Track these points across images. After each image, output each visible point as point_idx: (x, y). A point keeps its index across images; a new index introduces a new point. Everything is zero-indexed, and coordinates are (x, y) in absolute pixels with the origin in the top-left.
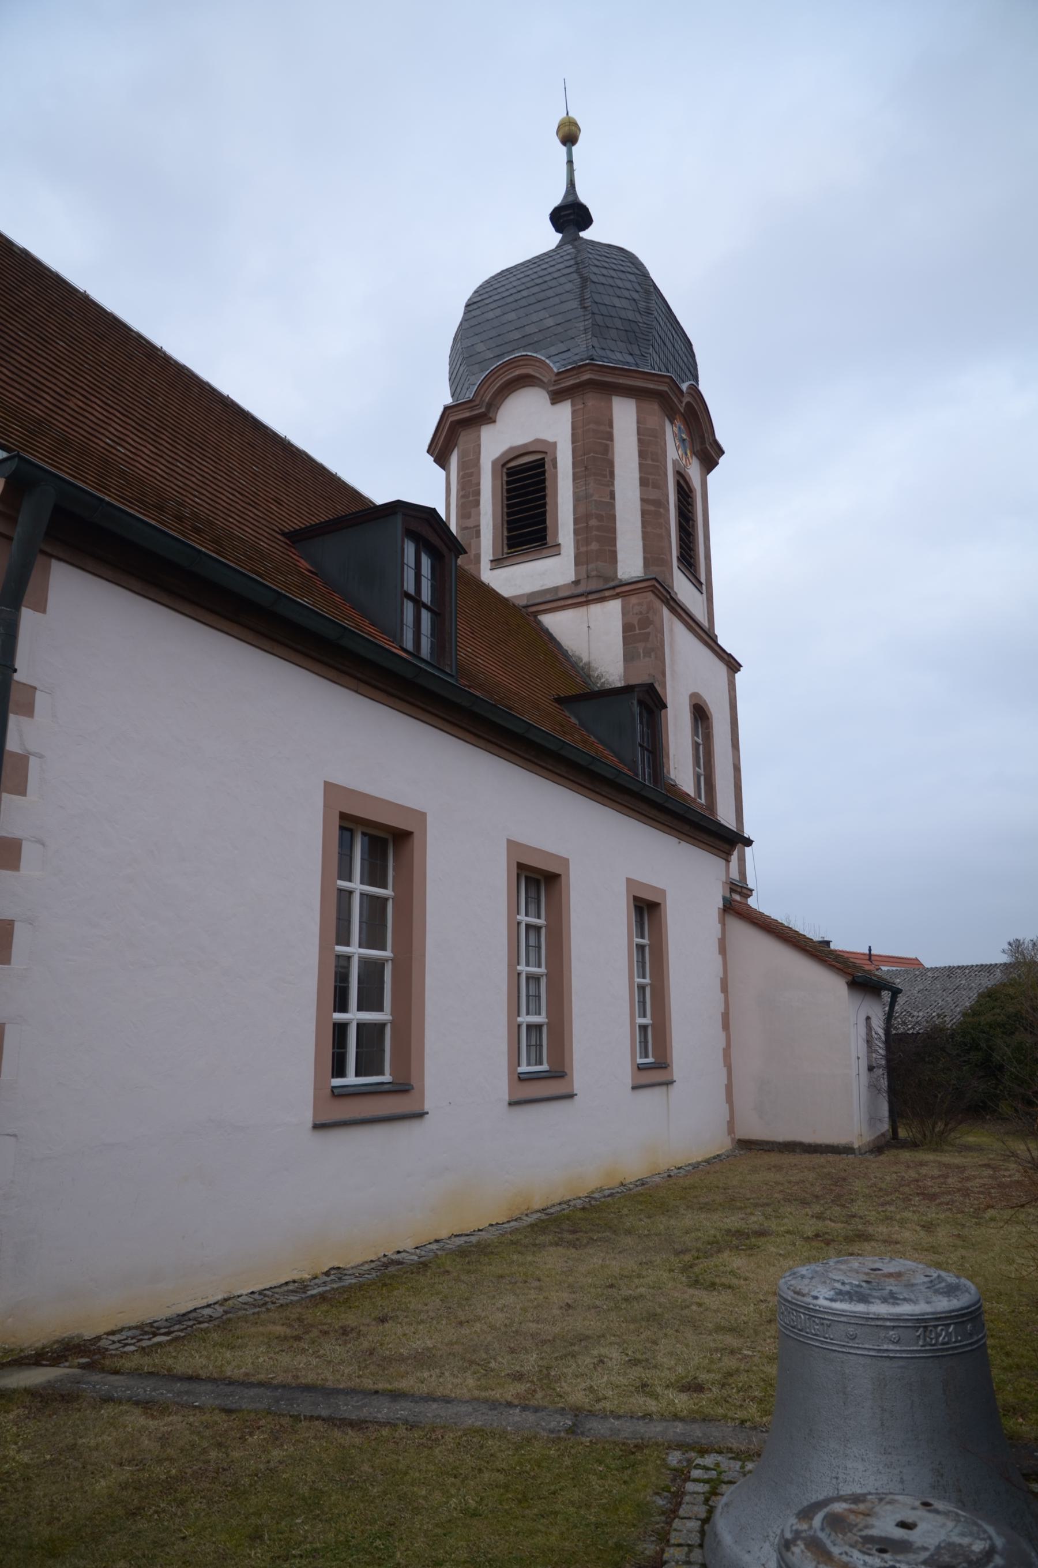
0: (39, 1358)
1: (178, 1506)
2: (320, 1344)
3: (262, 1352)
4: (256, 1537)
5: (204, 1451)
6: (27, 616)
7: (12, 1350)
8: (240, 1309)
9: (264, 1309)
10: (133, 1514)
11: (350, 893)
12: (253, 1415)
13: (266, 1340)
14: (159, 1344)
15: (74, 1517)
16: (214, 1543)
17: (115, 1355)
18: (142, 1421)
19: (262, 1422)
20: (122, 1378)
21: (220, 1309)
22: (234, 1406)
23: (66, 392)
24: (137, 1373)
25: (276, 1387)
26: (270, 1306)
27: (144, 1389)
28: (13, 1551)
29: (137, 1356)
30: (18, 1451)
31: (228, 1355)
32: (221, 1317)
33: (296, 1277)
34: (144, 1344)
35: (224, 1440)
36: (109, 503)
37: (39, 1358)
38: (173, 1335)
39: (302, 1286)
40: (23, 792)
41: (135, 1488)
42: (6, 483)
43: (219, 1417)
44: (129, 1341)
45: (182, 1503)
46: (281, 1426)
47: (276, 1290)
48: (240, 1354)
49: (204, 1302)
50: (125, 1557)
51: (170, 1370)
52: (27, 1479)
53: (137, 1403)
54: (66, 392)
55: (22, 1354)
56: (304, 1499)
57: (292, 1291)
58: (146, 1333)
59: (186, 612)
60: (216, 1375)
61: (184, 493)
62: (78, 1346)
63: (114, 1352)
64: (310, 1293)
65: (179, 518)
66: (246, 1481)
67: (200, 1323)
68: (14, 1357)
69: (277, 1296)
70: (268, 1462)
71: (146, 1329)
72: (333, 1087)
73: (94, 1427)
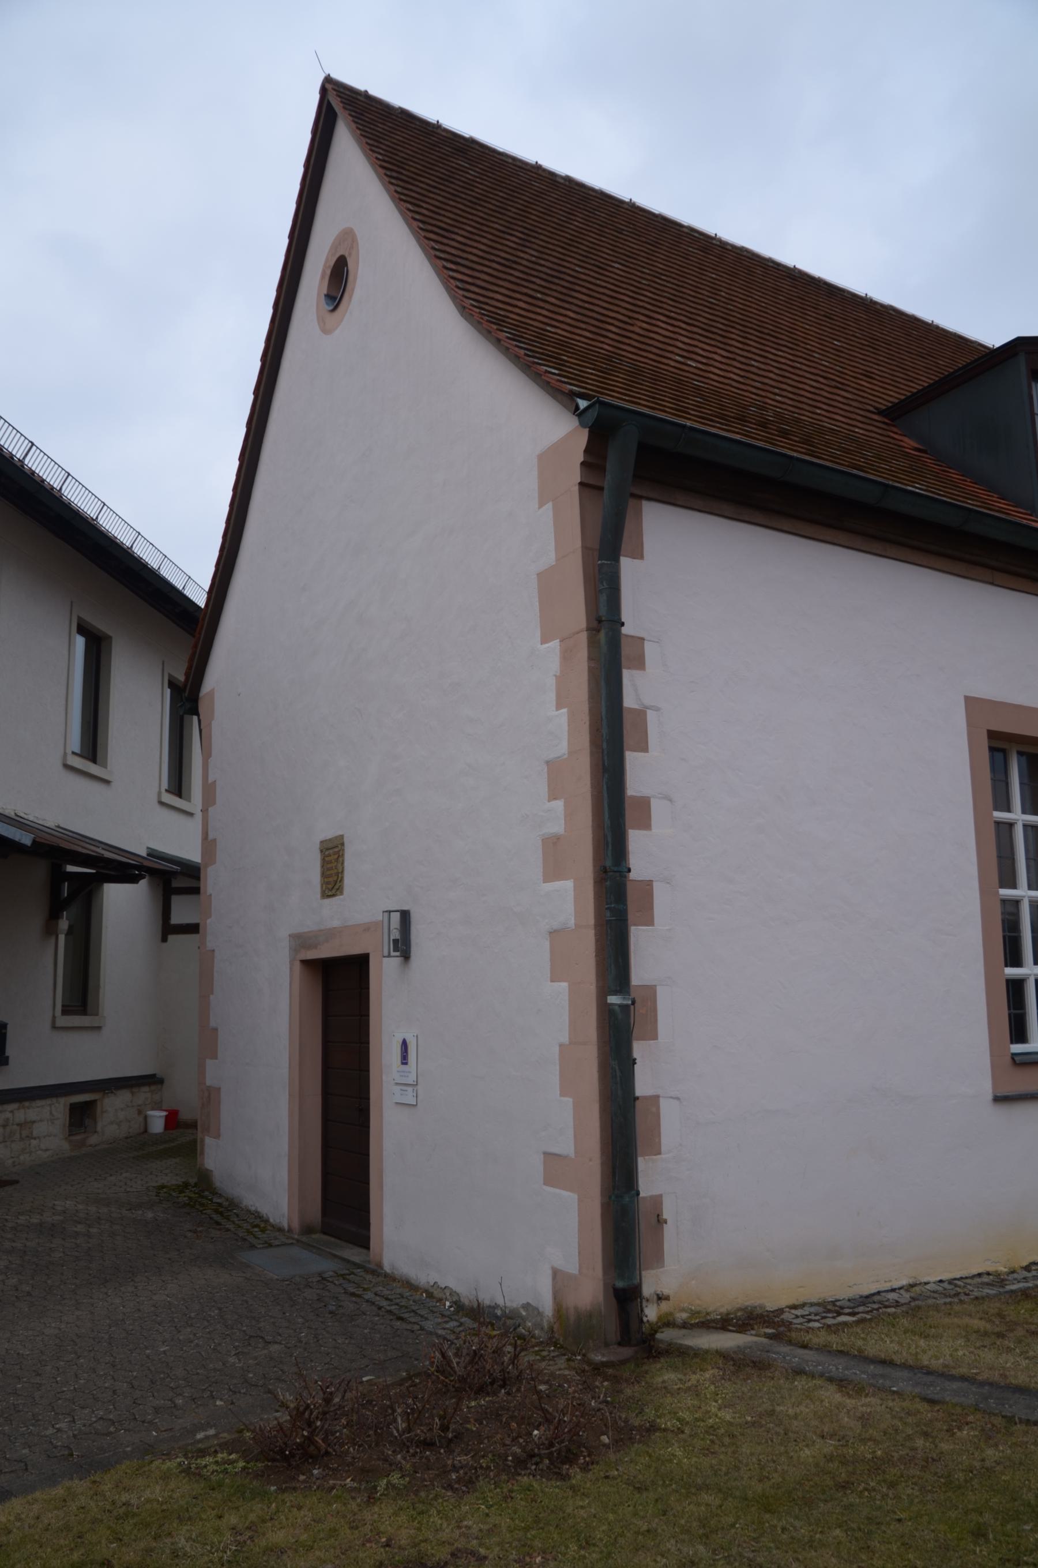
0: (724, 1323)
1: (888, 1488)
2: (1028, 1345)
3: (960, 1346)
4: (979, 1533)
5: (909, 1438)
6: (626, 564)
7: (699, 1312)
8: (929, 1297)
9: (956, 1300)
10: (844, 1486)
11: (1011, 825)
12: (959, 1410)
13: (964, 1334)
14: (845, 1324)
15: (784, 1479)
16: (933, 1531)
17: (801, 1330)
18: (838, 1397)
19: (971, 1418)
20: (811, 1352)
21: (906, 1297)
22: (936, 1397)
23: (630, 317)
24: (824, 1349)
25: (982, 1384)
26: (963, 1297)
27: (837, 1367)
28: (730, 1499)
29: (823, 1333)
30: (720, 1409)
31: (922, 1343)
32: (909, 1303)
33: (991, 1269)
34: (830, 1321)
35: (930, 1430)
36: (691, 429)
37: (724, 1323)
38: (859, 1316)
39: (998, 1280)
40: (645, 749)
41: (841, 1462)
42: (590, 432)
43: (923, 1407)
44: (813, 1317)
45: (892, 1485)
46: (993, 1425)
47: (969, 1281)
48: (936, 1344)
49: (887, 1286)
50: (840, 1527)
51: (860, 1351)
52: (733, 1436)
53: (831, 1380)
54: (630, 317)
55: (709, 1318)
56: (1029, 1505)
57: (987, 1284)
58: (829, 1311)
59: (785, 528)
60: (911, 1362)
61: (763, 394)
62: (761, 1316)
63: (799, 1326)
64: (1008, 1288)
65: (763, 425)
66: (961, 1476)
67: (886, 1307)
68: (702, 1320)
69: (971, 1288)
70: (983, 1460)
71: (829, 1307)
72: (1013, 1054)
73: (790, 1396)
